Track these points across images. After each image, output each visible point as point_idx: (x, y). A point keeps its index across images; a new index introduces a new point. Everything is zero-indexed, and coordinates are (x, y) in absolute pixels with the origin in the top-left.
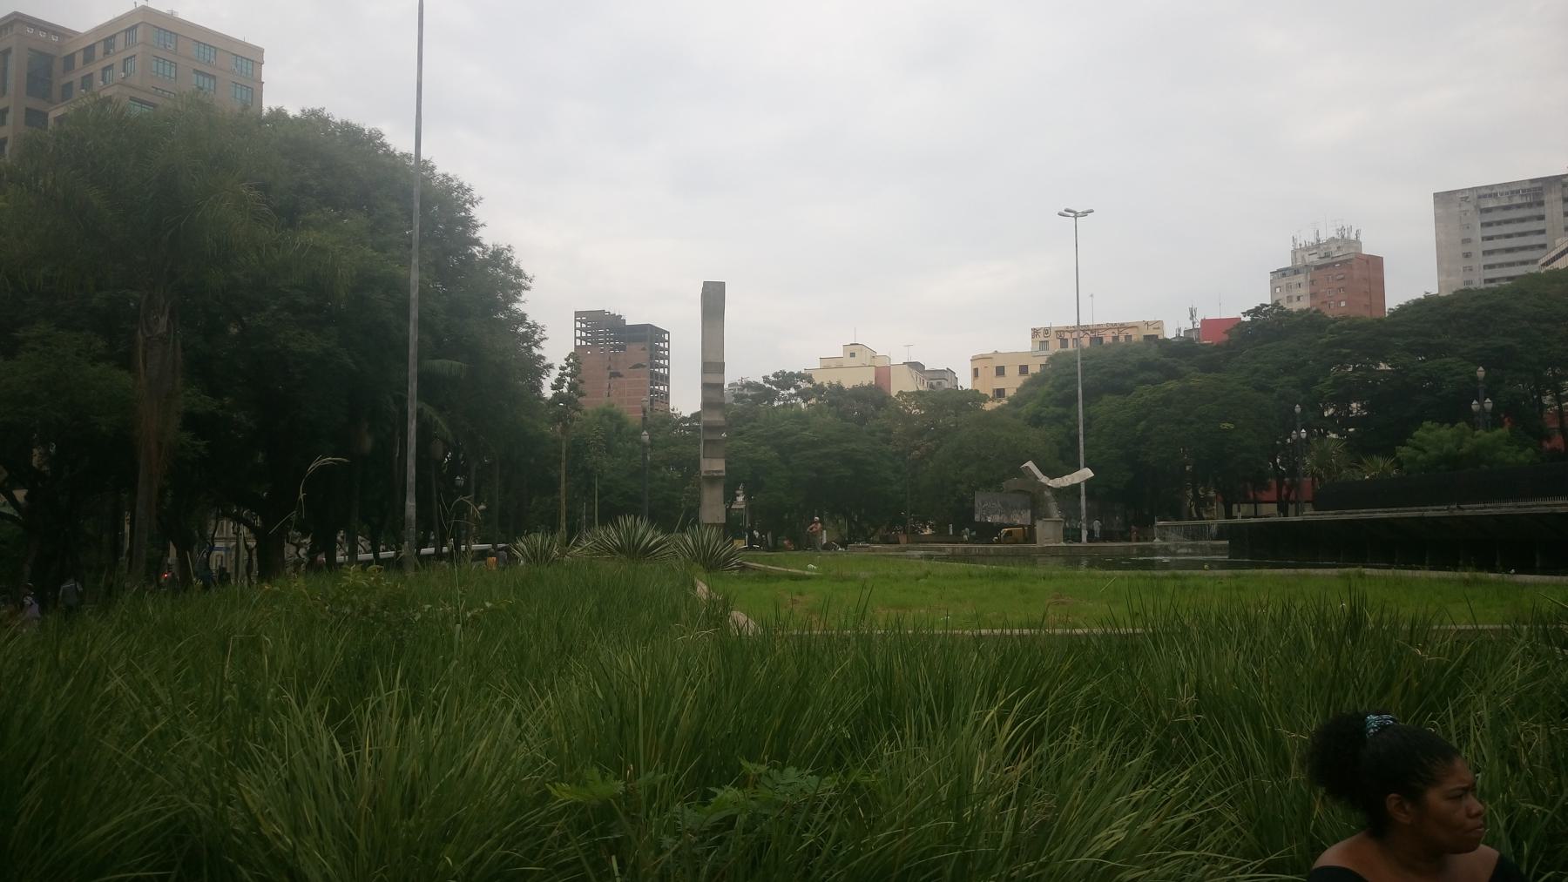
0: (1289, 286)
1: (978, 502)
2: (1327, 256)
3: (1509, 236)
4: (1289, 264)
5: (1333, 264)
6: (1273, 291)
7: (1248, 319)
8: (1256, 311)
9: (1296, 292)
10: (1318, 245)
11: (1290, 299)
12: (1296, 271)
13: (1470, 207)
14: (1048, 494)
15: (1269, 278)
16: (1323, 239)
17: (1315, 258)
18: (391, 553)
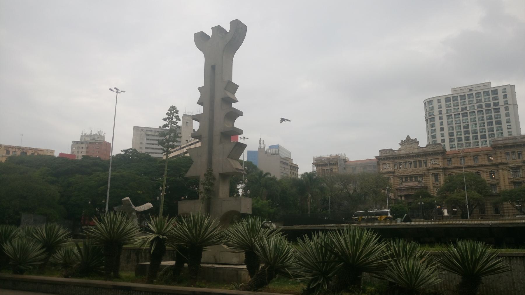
0: (78, 148)
1: (23, 218)
2: (93, 139)
3: (153, 144)
4: (79, 140)
5: (95, 143)
6: (72, 148)
7: (123, 153)
8: (126, 151)
9: (81, 150)
10: (91, 135)
11: (78, 152)
12: (82, 143)
13: (143, 133)
14: (134, 214)
15: (71, 143)
16: (93, 134)
17: (89, 140)
18: (241, 192)
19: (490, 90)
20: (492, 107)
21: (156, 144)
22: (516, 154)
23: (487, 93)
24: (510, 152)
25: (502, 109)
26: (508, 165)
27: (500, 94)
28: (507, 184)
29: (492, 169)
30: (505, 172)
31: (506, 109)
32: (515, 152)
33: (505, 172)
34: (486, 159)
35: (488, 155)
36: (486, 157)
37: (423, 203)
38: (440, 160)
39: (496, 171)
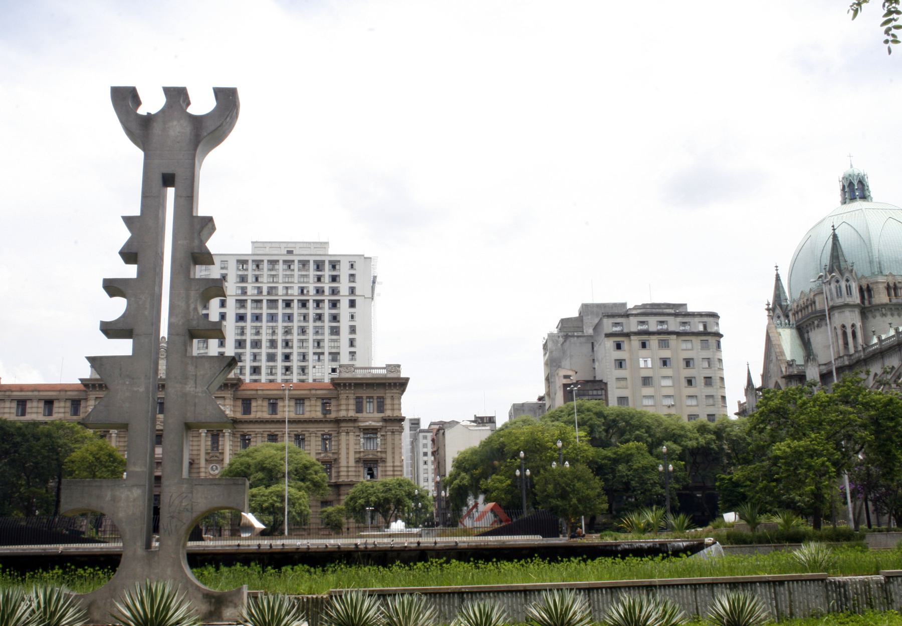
19: (327, 259)
20: (327, 297)
21: (223, 304)
22: (375, 401)
23: (319, 266)
24: (365, 396)
25: (344, 304)
26: (356, 425)
27: (344, 272)
28: (352, 462)
29: (326, 430)
30: (352, 437)
31: (352, 304)
32: (372, 397)
33: (352, 437)
34: (319, 409)
35: (323, 399)
36: (319, 403)
37: (528, 472)
38: (228, 402)
39: (334, 434)
